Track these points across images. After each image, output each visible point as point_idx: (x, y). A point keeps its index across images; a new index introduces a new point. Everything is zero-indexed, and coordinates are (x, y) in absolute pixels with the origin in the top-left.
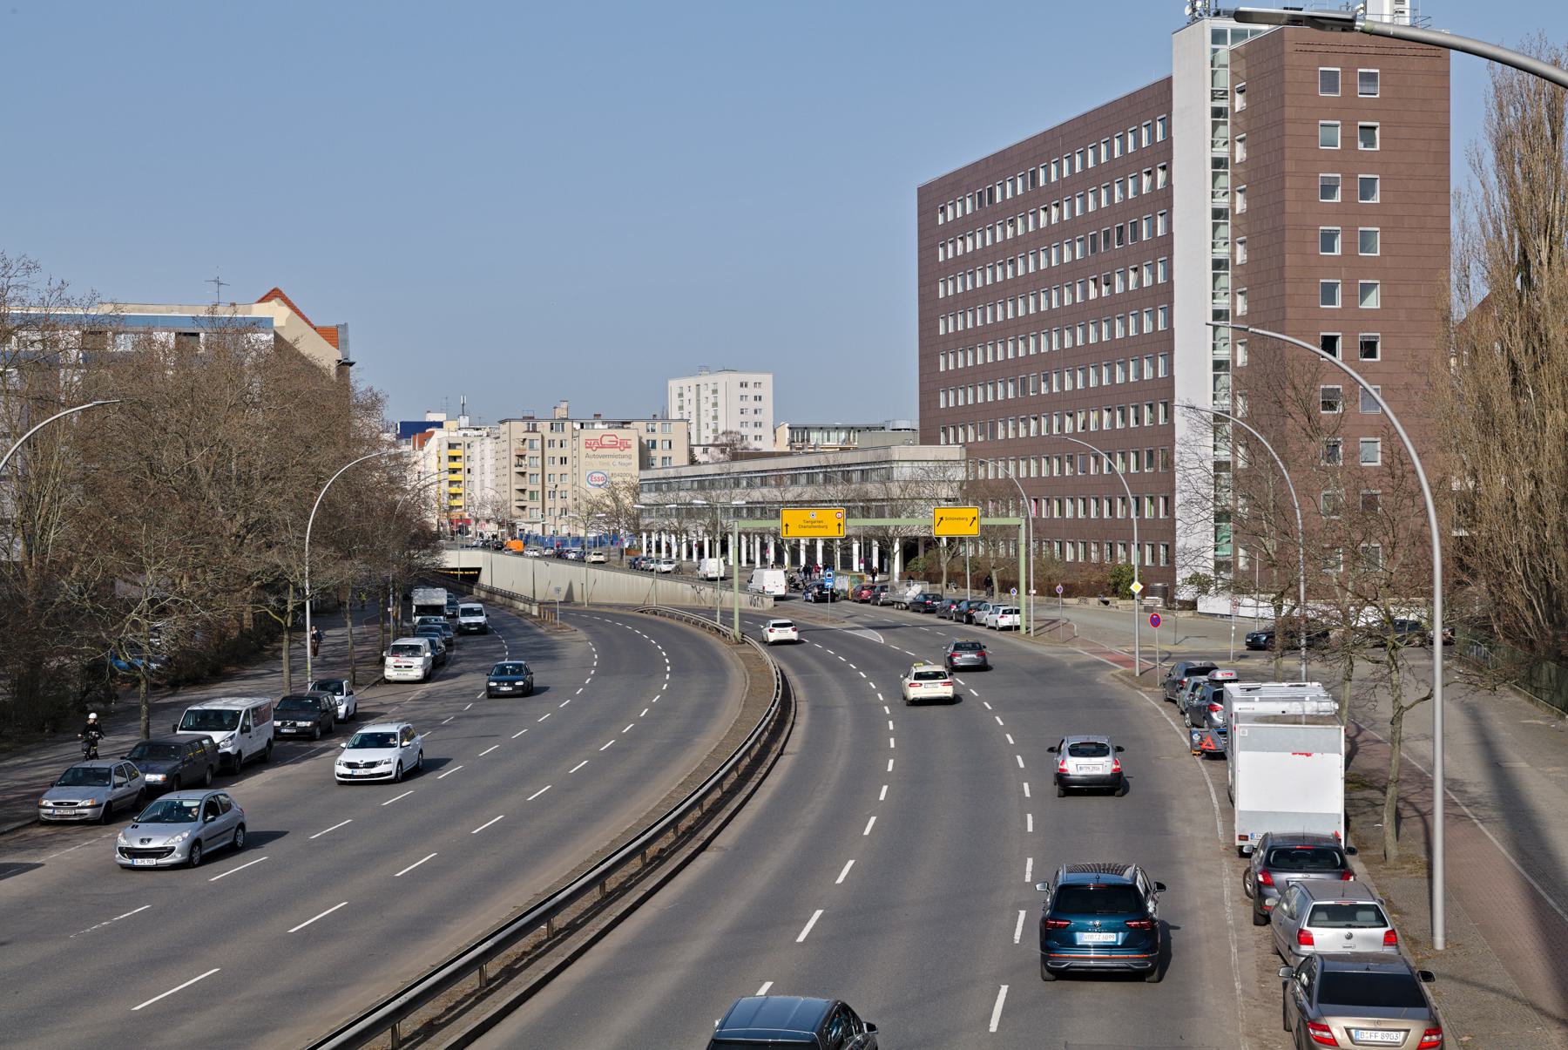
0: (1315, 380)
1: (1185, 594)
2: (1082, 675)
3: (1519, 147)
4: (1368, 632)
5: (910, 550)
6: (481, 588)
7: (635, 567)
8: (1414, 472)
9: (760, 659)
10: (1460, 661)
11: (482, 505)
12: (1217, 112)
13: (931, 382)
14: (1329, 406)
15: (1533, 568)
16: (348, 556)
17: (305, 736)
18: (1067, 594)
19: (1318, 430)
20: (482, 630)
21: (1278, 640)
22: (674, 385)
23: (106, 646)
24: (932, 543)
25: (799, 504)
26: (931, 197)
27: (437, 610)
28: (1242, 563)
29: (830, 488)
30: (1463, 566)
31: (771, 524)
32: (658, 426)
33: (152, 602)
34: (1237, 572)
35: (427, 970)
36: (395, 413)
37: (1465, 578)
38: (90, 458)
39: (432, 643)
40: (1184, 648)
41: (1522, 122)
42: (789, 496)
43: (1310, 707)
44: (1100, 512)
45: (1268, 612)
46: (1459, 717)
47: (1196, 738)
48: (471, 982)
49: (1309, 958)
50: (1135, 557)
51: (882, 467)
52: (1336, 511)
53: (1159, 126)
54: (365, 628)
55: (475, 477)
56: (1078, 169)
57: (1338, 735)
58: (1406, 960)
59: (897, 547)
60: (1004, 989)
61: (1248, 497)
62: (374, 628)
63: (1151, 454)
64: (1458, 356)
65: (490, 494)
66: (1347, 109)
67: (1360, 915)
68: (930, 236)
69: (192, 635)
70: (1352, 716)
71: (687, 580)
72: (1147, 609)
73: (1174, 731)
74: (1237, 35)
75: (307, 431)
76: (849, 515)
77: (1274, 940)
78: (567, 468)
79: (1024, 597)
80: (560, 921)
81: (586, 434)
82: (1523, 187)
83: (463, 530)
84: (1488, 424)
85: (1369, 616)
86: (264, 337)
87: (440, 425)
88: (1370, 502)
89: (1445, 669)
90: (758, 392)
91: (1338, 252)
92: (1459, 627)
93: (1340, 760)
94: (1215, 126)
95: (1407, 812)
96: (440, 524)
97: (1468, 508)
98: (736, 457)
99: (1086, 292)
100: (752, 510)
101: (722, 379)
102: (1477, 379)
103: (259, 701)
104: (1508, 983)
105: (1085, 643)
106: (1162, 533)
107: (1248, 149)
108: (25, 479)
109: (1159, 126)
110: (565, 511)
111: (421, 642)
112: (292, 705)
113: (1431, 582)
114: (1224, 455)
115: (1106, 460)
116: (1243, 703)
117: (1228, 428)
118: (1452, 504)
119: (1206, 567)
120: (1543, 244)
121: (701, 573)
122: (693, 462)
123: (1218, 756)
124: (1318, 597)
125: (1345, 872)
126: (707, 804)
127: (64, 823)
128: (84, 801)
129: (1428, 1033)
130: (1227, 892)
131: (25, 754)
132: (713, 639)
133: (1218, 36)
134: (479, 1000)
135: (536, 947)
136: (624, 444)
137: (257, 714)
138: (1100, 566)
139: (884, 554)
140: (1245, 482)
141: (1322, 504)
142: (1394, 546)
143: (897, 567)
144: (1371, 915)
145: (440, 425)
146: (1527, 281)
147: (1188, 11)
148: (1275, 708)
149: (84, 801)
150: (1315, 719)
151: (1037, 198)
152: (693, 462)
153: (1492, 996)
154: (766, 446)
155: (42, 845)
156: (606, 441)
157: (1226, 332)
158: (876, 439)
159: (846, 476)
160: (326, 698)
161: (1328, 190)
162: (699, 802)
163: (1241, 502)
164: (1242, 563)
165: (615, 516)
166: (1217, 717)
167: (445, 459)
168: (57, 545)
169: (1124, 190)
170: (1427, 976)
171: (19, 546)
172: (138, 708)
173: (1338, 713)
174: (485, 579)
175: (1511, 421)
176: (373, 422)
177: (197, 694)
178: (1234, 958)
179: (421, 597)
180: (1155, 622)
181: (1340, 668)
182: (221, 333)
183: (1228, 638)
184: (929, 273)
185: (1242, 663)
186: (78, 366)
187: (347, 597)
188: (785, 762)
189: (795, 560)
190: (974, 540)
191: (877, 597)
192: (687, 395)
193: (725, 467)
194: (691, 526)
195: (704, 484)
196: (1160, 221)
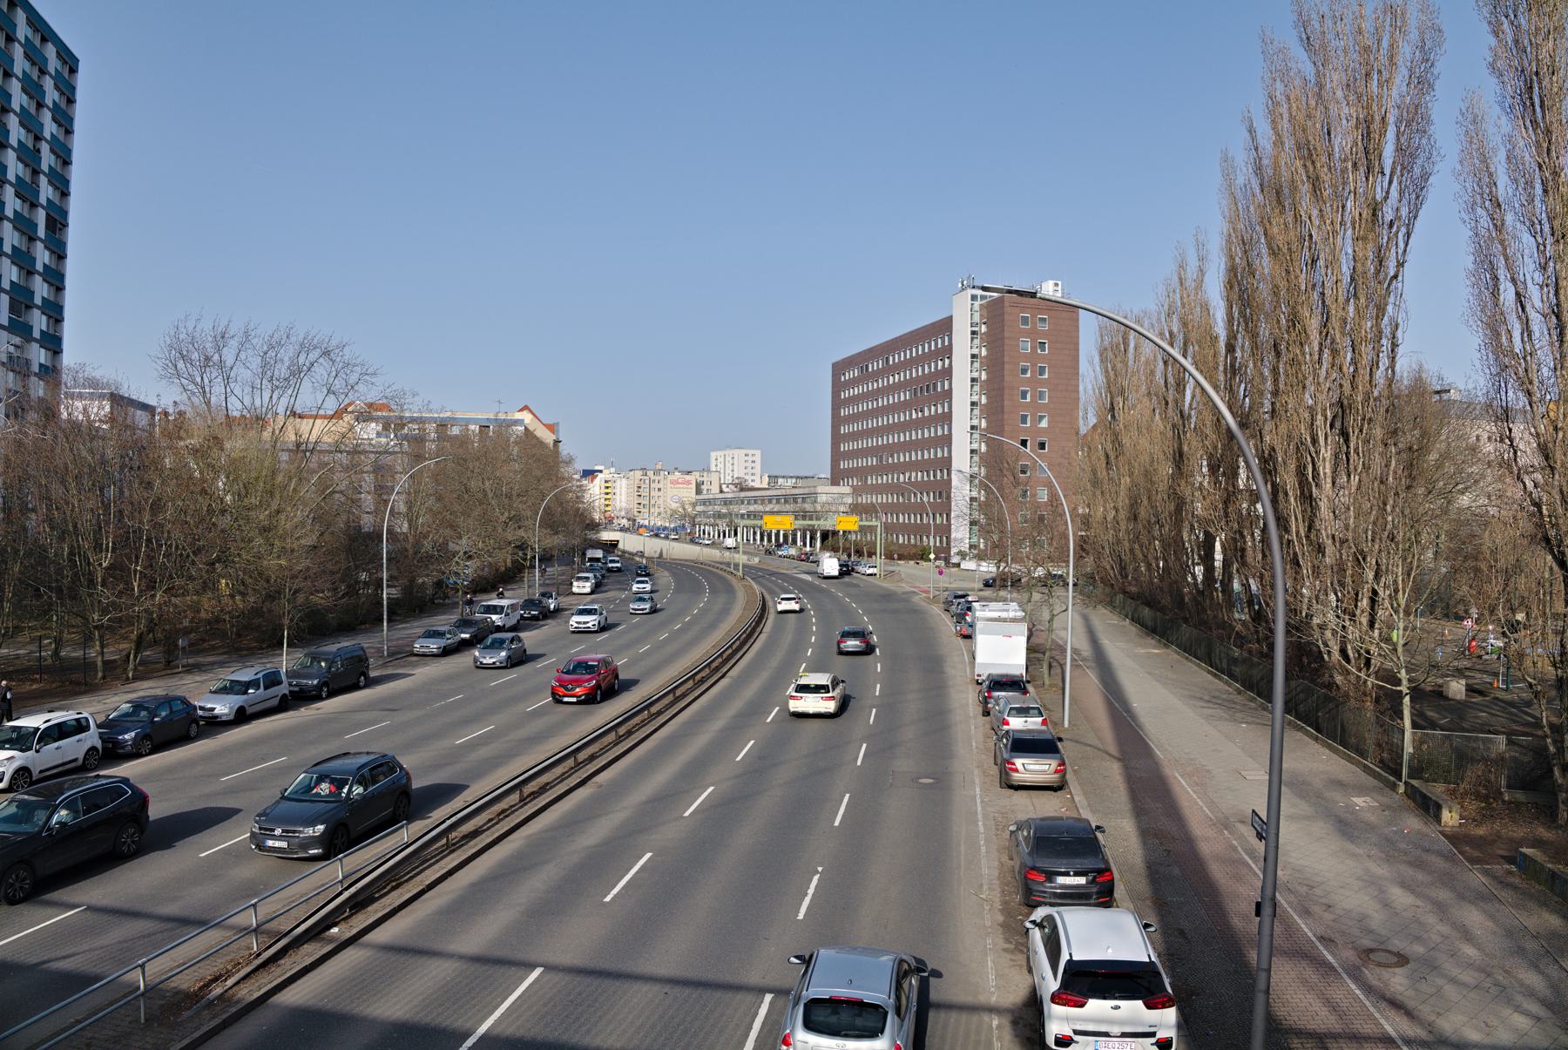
0: (1017, 460)
1: (955, 560)
2: (905, 598)
3: (1110, 354)
4: (1039, 579)
5: (825, 536)
6: (619, 550)
7: (692, 541)
8: (1062, 504)
9: (751, 587)
10: (1081, 594)
11: (620, 510)
12: (973, 333)
13: (837, 456)
14: (1024, 472)
15: (1114, 551)
16: (557, 533)
17: (534, 618)
18: (899, 559)
19: (1018, 484)
20: (619, 570)
21: (998, 582)
22: (713, 455)
23: (444, 573)
24: (835, 533)
25: (772, 513)
26: (839, 368)
27: (598, 560)
28: (982, 546)
29: (787, 506)
30: (1083, 549)
31: (758, 523)
32: (705, 474)
33: (465, 553)
34: (980, 550)
35: (590, 730)
36: (580, 465)
37: (1084, 555)
38: (439, 484)
39: (595, 576)
40: (953, 586)
41: (1111, 343)
42: (767, 509)
43: (1012, 614)
44: (916, 520)
45: (994, 569)
46: (1078, 618)
47: (958, 628)
48: (612, 737)
49: (1007, 732)
50: (932, 542)
51: (812, 496)
52: (1026, 522)
53: (946, 338)
54: (563, 568)
55: (617, 497)
56: (933, 348)
57: (1024, 627)
58: (1050, 732)
59: (819, 535)
60: (864, 746)
61: (986, 514)
62: (568, 568)
63: (940, 493)
64: (1083, 450)
65: (624, 505)
66: (1033, 334)
67: (1031, 711)
68: (837, 386)
69: (483, 569)
70: (1031, 619)
71: (717, 548)
72: (937, 567)
73: (948, 626)
74: (983, 297)
75: (539, 473)
76: (796, 519)
77: (991, 722)
78: (660, 494)
79: (879, 560)
80: (654, 709)
81: (670, 477)
82: (1112, 374)
83: (611, 522)
84: (1096, 483)
85: (1040, 572)
86: (520, 428)
87: (601, 471)
88: (1041, 518)
89: (1074, 597)
90: (754, 459)
91: (1028, 400)
92: (1081, 577)
93: (1024, 639)
94: (972, 339)
95: (1054, 664)
96: (600, 519)
97: (1086, 522)
98: (742, 490)
99: (911, 415)
100: (748, 515)
101: (736, 452)
102: (1090, 461)
103: (514, 601)
104: (1096, 742)
105: (907, 582)
106: (945, 530)
107: (987, 350)
108: (409, 494)
109: (946, 338)
110: (659, 514)
111: (590, 575)
112: (529, 604)
113: (1068, 556)
114: (975, 494)
115: (919, 495)
116: (981, 612)
117: (977, 481)
118: (1079, 520)
119: (965, 547)
120: (1120, 400)
121: (724, 545)
122: (721, 491)
123: (968, 637)
124: (1016, 562)
125: (1025, 692)
126: (725, 656)
127: (424, 655)
128: (433, 646)
129: (1060, 765)
130: (970, 701)
131: (407, 622)
132: (729, 577)
133: (974, 298)
134: (615, 745)
135: (643, 721)
136: (689, 483)
137: (512, 606)
138: (915, 545)
139: (812, 538)
140: (985, 507)
141: (1020, 519)
142: (1052, 539)
143: (818, 544)
144: (1036, 712)
145: (601, 471)
146: (1113, 417)
147: (960, 285)
148: (995, 615)
149: (433, 646)
150: (1014, 620)
151: (889, 370)
152: (721, 491)
153: (1089, 748)
154: (757, 485)
155: (414, 665)
156: (680, 481)
157: (976, 436)
158: (809, 482)
159: (795, 501)
160: (544, 600)
161: (1024, 371)
162: (721, 655)
163: (982, 517)
164: (982, 546)
165: (683, 517)
166: (968, 619)
167: (603, 488)
168: (423, 525)
169: (930, 367)
170: (1060, 740)
171: (406, 525)
172: (458, 603)
173: (1025, 617)
174: (621, 546)
175: (1106, 482)
176: (570, 469)
177: (485, 597)
178: (973, 732)
179: (591, 553)
180: (941, 573)
181: (1026, 596)
182: (500, 426)
183: (974, 581)
184: (837, 404)
185: (982, 593)
186: (434, 441)
187: (555, 553)
188: (763, 637)
189: (770, 540)
190: (855, 532)
191: (808, 558)
192: (719, 460)
193: (737, 495)
194: (720, 523)
195: (726, 502)
196: (946, 383)
